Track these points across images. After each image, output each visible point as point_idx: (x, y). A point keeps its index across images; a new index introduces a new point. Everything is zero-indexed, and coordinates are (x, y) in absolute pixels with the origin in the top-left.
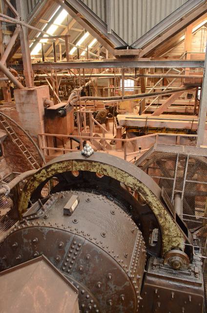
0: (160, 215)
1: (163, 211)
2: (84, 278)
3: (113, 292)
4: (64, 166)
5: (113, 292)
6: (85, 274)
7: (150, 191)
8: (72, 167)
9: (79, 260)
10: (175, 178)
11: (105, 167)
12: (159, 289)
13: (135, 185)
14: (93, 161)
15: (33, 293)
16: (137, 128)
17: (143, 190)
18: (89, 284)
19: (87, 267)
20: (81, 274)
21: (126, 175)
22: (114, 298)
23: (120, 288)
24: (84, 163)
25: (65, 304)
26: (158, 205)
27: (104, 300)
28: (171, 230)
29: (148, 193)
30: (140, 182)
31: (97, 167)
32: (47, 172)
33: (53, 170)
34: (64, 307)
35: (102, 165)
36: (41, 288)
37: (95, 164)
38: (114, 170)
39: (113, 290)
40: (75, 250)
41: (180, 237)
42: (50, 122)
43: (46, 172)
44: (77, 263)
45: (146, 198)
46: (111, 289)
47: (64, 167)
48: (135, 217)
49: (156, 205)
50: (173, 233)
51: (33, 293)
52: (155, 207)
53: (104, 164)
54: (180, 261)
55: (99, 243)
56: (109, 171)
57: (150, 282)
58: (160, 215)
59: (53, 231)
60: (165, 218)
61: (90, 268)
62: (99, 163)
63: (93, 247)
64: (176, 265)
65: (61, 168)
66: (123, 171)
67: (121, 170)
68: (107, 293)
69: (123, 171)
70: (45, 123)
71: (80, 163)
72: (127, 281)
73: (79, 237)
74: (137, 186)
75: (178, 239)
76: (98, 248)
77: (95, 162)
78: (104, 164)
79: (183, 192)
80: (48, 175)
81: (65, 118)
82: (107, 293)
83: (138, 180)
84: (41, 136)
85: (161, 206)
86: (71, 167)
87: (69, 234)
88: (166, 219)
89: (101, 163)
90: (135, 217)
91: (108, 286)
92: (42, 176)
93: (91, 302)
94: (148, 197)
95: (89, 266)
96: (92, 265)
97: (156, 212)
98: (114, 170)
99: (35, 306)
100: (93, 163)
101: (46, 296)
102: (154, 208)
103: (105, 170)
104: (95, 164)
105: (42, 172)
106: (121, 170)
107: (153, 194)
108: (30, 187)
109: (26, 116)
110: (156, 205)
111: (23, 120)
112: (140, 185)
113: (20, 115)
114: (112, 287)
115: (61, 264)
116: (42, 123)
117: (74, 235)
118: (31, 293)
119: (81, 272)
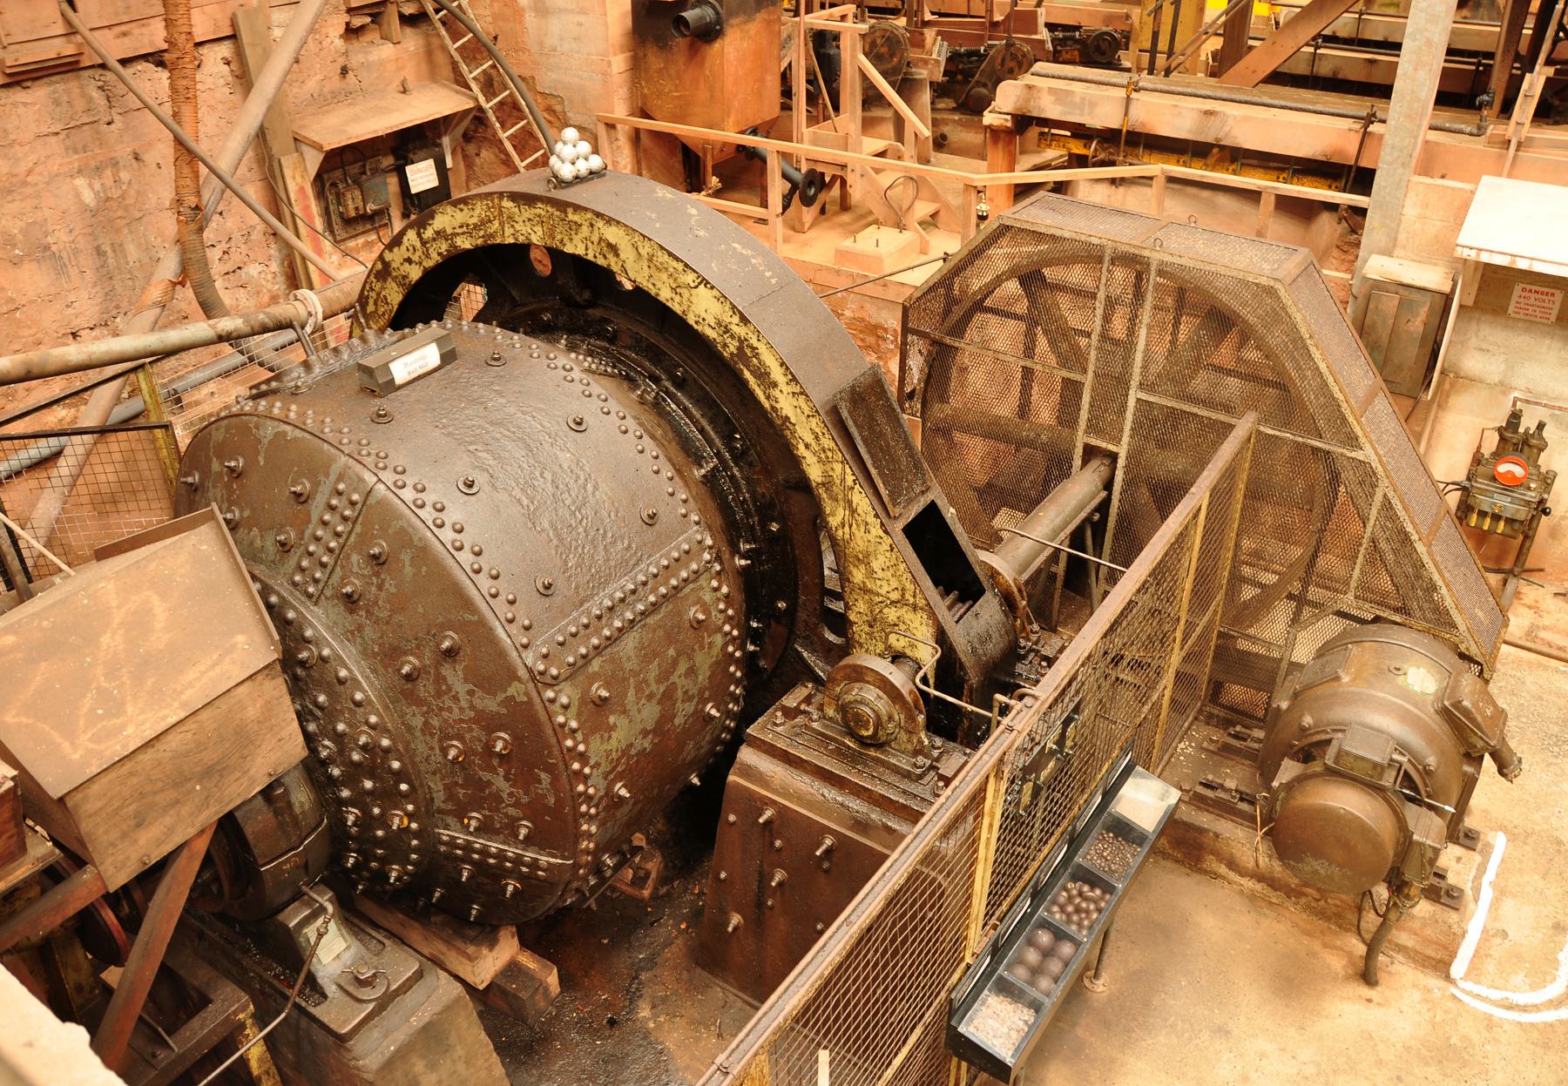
0: (827, 484)
1: (838, 467)
2: (360, 628)
3: (461, 709)
4: (475, 220)
5: (461, 709)
6: (363, 613)
7: (782, 364)
8: (502, 224)
9: (348, 557)
10: (1090, 374)
11: (613, 234)
12: (782, 811)
13: (727, 331)
14: (568, 204)
15: (119, 607)
16: (1081, 132)
17: (757, 356)
18: (375, 655)
19: (374, 589)
20: (352, 612)
21: (690, 278)
22: (468, 736)
23: (491, 705)
24: (541, 209)
25: (212, 667)
26: (817, 438)
27: (432, 735)
28: (876, 565)
29: (777, 374)
30: (744, 320)
31: (585, 230)
32: (424, 243)
33: (440, 234)
34: (203, 673)
35: (600, 224)
36: (156, 600)
37: (576, 218)
38: (645, 250)
39: (463, 704)
40: (337, 518)
41: (915, 608)
42: (655, 61)
43: (418, 244)
44: (343, 567)
45: (768, 398)
46: (456, 698)
47: (475, 226)
48: (760, 490)
49: (809, 438)
50: (886, 587)
51: (119, 607)
52: (807, 446)
53: (609, 221)
54: (883, 712)
55: (429, 508)
56: (627, 253)
57: (748, 772)
58: (827, 484)
59: (284, 433)
60: (850, 503)
61: (383, 594)
62: (589, 215)
63: (401, 516)
64: (860, 720)
65: (469, 230)
66: (677, 259)
67: (670, 254)
68: (441, 709)
69: (677, 259)
70: (637, 66)
71: (528, 212)
72: (519, 680)
73: (358, 468)
74: (732, 337)
75: (908, 615)
76: (419, 523)
77: (578, 208)
78: (609, 221)
79: (1122, 451)
80: (428, 256)
81: (717, 45)
82: (441, 709)
83: (733, 307)
84: (611, 126)
85: (827, 442)
86: (496, 223)
87: (333, 451)
88: (853, 511)
89: (598, 215)
90: (760, 490)
91: (444, 678)
92: (409, 261)
93: (367, 723)
94: (776, 393)
95: (380, 587)
96: (390, 586)
97: (814, 473)
98: (645, 250)
99: (105, 639)
100: (572, 216)
101: (159, 625)
102: (801, 447)
103: (613, 248)
104: (576, 218)
105: (405, 239)
106: (670, 254)
107: (794, 379)
108: (375, 303)
109: (555, 25)
110: (809, 438)
111: (541, 44)
112: (740, 331)
113: (530, 19)
114: (461, 688)
115: (292, 562)
116: (619, 63)
117: (344, 459)
118: (114, 603)
119: (350, 601)
